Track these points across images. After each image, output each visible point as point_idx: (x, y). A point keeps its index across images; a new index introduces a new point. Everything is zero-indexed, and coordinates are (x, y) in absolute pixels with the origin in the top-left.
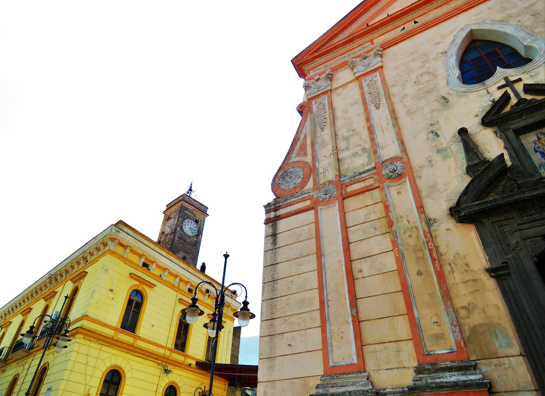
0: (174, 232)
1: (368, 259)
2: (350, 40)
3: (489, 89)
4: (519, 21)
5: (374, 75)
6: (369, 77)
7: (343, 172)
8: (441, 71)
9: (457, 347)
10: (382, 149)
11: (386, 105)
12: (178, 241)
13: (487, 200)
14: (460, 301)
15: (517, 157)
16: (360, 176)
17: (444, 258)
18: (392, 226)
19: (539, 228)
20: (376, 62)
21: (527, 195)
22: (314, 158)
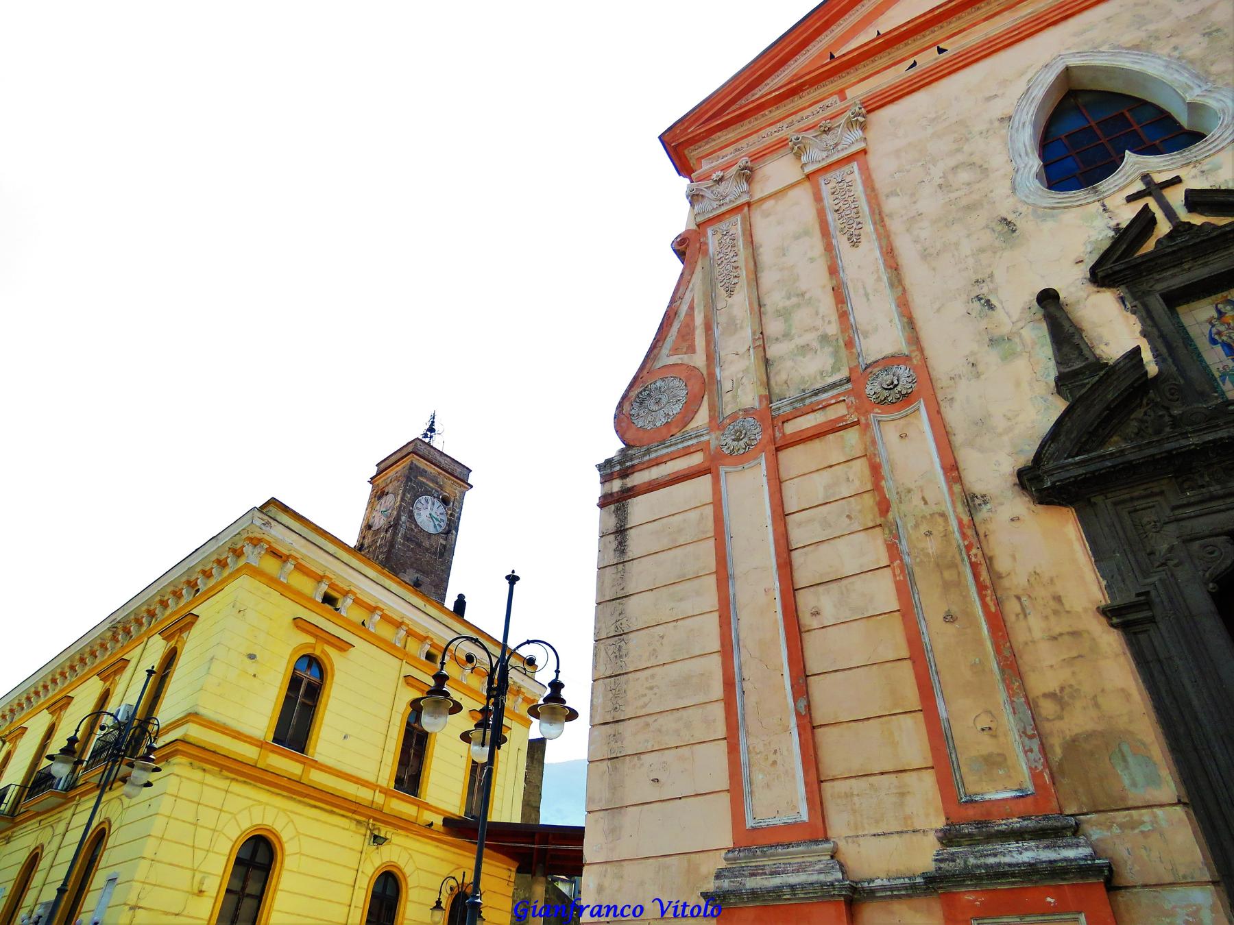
0: (394, 525)
1: (834, 585)
2: (793, 91)
3: (1106, 202)
4: (1175, 48)
5: (847, 169)
6: (836, 175)
7: (776, 390)
8: (998, 161)
9: (1035, 786)
10: (866, 337)
11: (874, 237)
12: (403, 545)
13: (1101, 452)
14: (1043, 681)
15: (1170, 355)
16: (814, 399)
17: (1006, 583)
18: (887, 511)
19: (1221, 516)
20: (851, 141)
21: (1193, 440)
22: (711, 357)
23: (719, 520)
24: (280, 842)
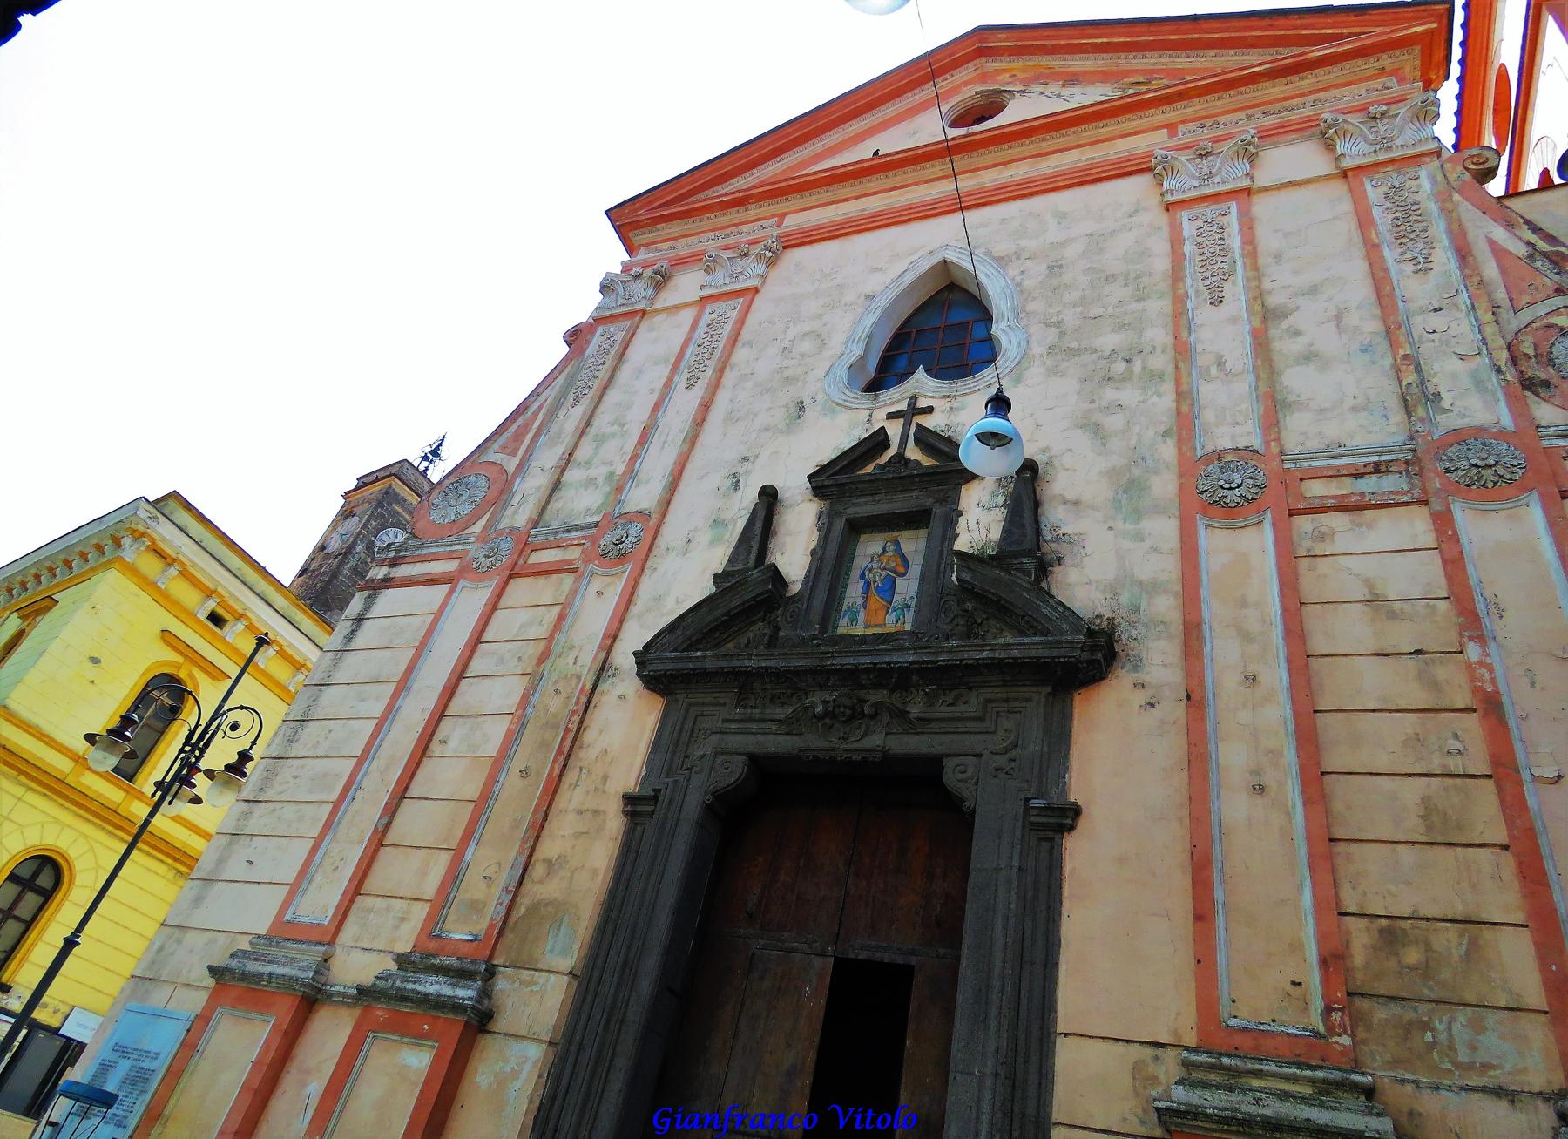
0: (347, 552)
2: (740, 202)
5: (733, 303)
7: (547, 516)
12: (349, 578)
14: (549, 848)
17: (582, 754)
19: (750, 738)
21: (753, 663)
22: (520, 467)
23: (430, 631)
24: (70, 869)
